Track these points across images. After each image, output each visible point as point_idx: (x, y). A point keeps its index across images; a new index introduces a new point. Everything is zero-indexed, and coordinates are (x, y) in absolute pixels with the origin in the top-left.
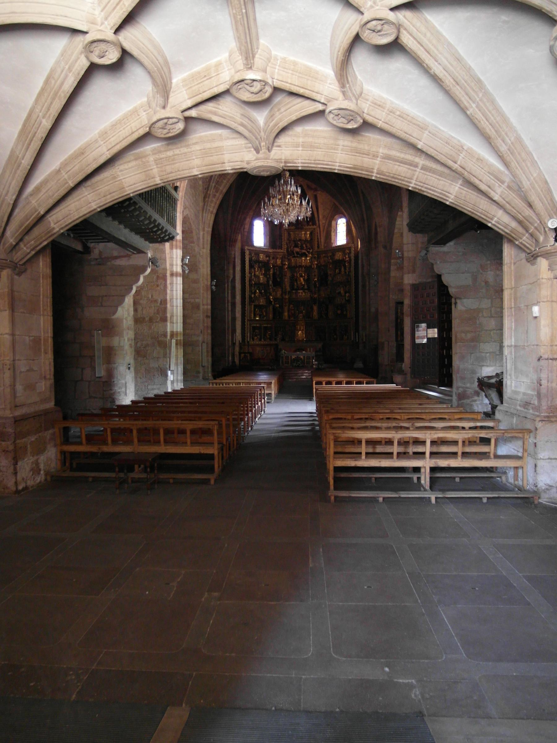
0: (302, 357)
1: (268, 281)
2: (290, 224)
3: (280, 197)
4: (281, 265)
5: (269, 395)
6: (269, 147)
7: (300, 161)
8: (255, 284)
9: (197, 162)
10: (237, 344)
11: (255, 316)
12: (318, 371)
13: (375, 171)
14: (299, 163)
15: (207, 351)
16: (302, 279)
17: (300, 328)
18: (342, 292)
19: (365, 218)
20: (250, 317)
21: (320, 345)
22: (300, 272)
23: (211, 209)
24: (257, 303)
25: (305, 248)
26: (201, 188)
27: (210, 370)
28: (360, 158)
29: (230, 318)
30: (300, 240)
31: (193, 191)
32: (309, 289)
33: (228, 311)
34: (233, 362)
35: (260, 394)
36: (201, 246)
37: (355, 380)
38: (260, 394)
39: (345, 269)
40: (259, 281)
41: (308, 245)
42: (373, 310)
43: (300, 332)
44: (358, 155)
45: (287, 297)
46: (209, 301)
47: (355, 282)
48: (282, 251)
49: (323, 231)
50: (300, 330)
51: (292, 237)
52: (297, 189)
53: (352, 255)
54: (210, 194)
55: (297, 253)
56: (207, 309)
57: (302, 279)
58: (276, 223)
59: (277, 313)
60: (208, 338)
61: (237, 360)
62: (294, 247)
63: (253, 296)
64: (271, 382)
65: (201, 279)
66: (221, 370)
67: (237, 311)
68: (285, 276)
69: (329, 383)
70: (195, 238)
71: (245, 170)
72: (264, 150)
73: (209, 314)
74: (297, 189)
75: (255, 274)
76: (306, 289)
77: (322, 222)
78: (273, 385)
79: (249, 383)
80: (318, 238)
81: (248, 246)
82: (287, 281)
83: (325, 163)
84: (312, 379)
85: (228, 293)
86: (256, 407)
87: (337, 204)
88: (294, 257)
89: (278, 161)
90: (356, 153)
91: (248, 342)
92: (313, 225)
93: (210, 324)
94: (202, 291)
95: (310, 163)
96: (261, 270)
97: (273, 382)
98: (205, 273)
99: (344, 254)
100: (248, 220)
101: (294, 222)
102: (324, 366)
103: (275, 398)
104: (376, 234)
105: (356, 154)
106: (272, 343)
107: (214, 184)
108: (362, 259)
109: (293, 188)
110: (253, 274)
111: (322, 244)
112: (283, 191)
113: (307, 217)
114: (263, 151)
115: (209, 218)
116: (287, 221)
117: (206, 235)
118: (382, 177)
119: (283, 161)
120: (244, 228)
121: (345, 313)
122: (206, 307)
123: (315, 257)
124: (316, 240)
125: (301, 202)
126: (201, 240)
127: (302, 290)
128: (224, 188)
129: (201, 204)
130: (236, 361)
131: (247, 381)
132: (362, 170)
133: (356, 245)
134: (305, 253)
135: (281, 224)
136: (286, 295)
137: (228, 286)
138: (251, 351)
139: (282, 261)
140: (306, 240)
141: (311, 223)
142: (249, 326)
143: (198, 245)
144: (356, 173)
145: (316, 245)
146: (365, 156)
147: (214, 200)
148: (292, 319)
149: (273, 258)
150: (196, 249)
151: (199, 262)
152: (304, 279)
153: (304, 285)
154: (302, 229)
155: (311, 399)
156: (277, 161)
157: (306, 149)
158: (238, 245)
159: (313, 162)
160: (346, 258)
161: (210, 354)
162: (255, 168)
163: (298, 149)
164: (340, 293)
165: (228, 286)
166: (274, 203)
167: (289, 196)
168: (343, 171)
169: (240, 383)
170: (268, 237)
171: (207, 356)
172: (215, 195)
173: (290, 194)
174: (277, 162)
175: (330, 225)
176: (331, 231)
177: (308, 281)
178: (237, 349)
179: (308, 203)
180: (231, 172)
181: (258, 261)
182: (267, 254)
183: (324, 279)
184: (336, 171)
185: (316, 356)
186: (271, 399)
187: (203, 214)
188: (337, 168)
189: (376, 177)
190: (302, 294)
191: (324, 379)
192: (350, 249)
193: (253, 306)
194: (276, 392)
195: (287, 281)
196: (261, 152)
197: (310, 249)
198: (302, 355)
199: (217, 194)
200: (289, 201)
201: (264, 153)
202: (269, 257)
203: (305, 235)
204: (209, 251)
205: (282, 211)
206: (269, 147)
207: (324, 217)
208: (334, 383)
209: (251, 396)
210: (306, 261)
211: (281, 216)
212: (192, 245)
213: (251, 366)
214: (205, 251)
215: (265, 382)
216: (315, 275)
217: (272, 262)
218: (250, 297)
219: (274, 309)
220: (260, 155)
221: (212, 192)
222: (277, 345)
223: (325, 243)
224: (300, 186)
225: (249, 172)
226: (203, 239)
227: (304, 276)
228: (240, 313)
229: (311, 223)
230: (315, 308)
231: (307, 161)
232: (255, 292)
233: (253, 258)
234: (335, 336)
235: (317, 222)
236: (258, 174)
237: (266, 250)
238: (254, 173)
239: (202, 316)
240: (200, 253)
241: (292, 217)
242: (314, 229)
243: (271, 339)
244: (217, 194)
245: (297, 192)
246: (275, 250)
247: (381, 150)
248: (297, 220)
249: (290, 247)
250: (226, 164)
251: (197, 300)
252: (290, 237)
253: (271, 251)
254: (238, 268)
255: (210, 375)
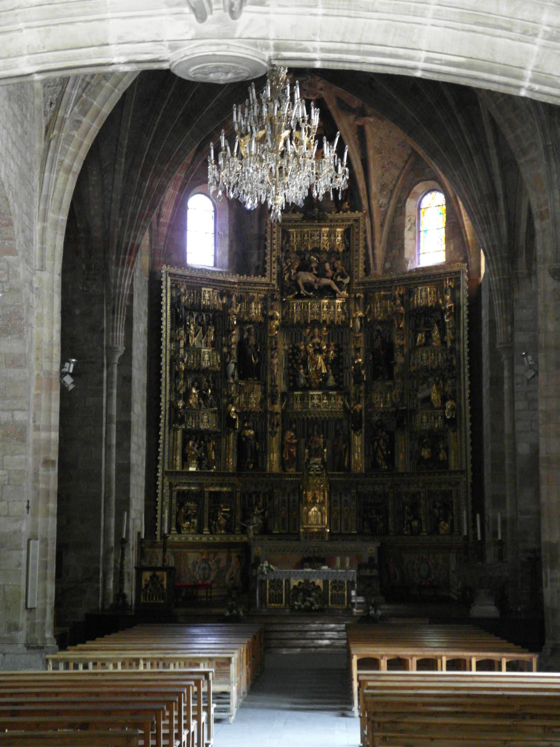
0: (319, 582)
1: (224, 364)
2: (289, 208)
3: (261, 133)
4: (261, 319)
5: (223, 696)
6: (232, 5)
7: (317, 45)
8: (188, 371)
9: (29, 38)
10: (133, 541)
11: (185, 461)
12: (367, 626)
13: (528, 74)
14: (315, 50)
15: (45, 565)
16: (320, 359)
17: (314, 498)
18: (435, 396)
19: (500, 191)
20: (172, 464)
21: (370, 549)
22: (317, 340)
23: (67, 161)
24: (191, 424)
25: (330, 273)
26: (38, 101)
27: (49, 619)
28: (487, 38)
29: (114, 466)
30: (316, 251)
31: (16, 107)
32: (340, 387)
33: (108, 447)
34: (120, 595)
35: (198, 693)
36: (37, 263)
37: (474, 657)
38: (198, 693)
39: (443, 331)
40: (199, 364)
41: (338, 264)
42: (523, 449)
43: (314, 509)
44: (480, 29)
45: (277, 408)
46: (55, 419)
47: (470, 370)
48: (263, 280)
49: (382, 226)
50: (314, 504)
51: (295, 240)
52: (309, 112)
53: (463, 295)
54: (63, 120)
55: (309, 286)
56: (49, 441)
57: (320, 359)
58: (248, 206)
59: (250, 455)
60: (49, 526)
61: (129, 590)
62: (298, 270)
63: (180, 404)
64: (229, 659)
65: (33, 356)
66: (83, 618)
67: (133, 447)
68: (274, 349)
69: (398, 663)
70: (20, 239)
71: (165, 66)
72: (218, 12)
73: (54, 456)
74: (309, 112)
75: (187, 344)
76: (332, 389)
77: (379, 201)
78: (233, 668)
79: (165, 663)
80: (366, 247)
81: (171, 264)
82: (278, 363)
83: (388, 50)
84: (347, 648)
85: (109, 395)
86: (184, 738)
87: (421, 152)
88: (299, 296)
89: (258, 43)
90: (476, 23)
91: (164, 537)
92: (353, 209)
93: (54, 485)
94: (33, 391)
95: (348, 52)
96: (204, 333)
97: (235, 658)
98: (46, 338)
99: (441, 291)
100: (170, 193)
101: (300, 203)
102: (385, 609)
103: (242, 707)
104: (531, 235)
105: (474, 27)
106: (232, 539)
107: (75, 93)
108: (491, 303)
109: (299, 111)
110: (182, 344)
111: (379, 262)
112: (271, 120)
113: (336, 192)
114: (216, 14)
115: (59, 186)
116: (281, 200)
117: (50, 233)
118: (546, 89)
119: (271, 43)
120: (159, 216)
121: (441, 456)
122: (43, 435)
123: (357, 299)
124: (362, 251)
125: (320, 147)
126: (37, 246)
127: (319, 388)
128: (104, 104)
129: (39, 146)
130: (126, 591)
131: (158, 655)
132: (491, 71)
133: (473, 268)
134: (328, 288)
135: (263, 209)
136: (273, 403)
137: (110, 375)
138: (171, 562)
139: (264, 308)
140: (333, 253)
141: (346, 205)
142: (166, 490)
143: (28, 262)
144: (476, 78)
145: (361, 267)
146: (499, 32)
147: (75, 133)
148: (292, 470)
149: (240, 300)
150: (21, 270)
151: (30, 306)
152: (326, 360)
153: (326, 378)
154: (322, 219)
155: (343, 709)
156: (254, 42)
157: (335, 12)
158: (143, 261)
159: (353, 47)
160: (445, 301)
161: (52, 571)
162: (193, 61)
163: (314, 11)
164: (428, 399)
165: (110, 375)
166: (242, 151)
167: (286, 134)
168: (439, 73)
169: (137, 661)
170: (227, 242)
171: (44, 578)
172: (79, 122)
173: (289, 127)
174: (255, 45)
175: (400, 210)
176: (403, 226)
177: (336, 365)
178: (131, 557)
179: (340, 152)
180: (127, 68)
181: (196, 308)
182: (224, 291)
183: (382, 360)
184: (419, 74)
185: (360, 578)
186: (226, 710)
187: (42, 172)
188: (421, 65)
189: (530, 90)
190: (320, 403)
191: (384, 653)
192: (456, 276)
193: (179, 433)
194: (244, 688)
195: (278, 363)
196: (209, 17)
197: (343, 277)
198: (318, 576)
199: (85, 120)
200: (285, 144)
201: (220, 20)
202: (229, 297)
203: (330, 236)
204: (57, 278)
205: (266, 172)
206: (232, 5)
207: (383, 187)
208: (413, 663)
209: (169, 704)
210: (331, 309)
211: (264, 186)
212: (10, 258)
213: (169, 607)
214: (46, 276)
215: (210, 659)
216: (357, 350)
217: (237, 311)
218: (173, 407)
219: (242, 444)
220: (209, 27)
221: (69, 112)
222: (246, 548)
223: (386, 260)
224: (320, 104)
225: (178, 73)
226: (43, 242)
227: (328, 352)
228: (144, 452)
229: (346, 205)
230: (358, 440)
231: (339, 46)
232: (188, 393)
233: (183, 299)
234: (415, 523)
235: (364, 202)
236: (200, 78)
237: (221, 278)
238: (190, 73)
239: (30, 459)
240: (31, 283)
241: (294, 191)
242: (356, 220)
243: (229, 530)
244: (85, 120)
245: (309, 121)
246: (244, 278)
247: (546, 17)
248: (309, 199)
249: (289, 270)
250: (113, 49)
251: (19, 416)
252: (288, 241)
253: (234, 279)
254: (140, 327)
255: (49, 635)
